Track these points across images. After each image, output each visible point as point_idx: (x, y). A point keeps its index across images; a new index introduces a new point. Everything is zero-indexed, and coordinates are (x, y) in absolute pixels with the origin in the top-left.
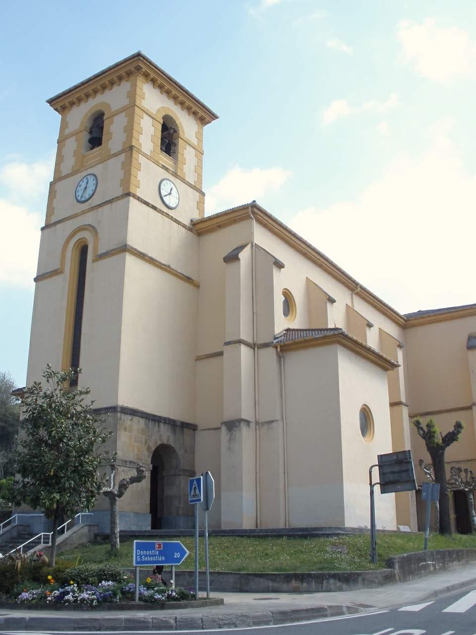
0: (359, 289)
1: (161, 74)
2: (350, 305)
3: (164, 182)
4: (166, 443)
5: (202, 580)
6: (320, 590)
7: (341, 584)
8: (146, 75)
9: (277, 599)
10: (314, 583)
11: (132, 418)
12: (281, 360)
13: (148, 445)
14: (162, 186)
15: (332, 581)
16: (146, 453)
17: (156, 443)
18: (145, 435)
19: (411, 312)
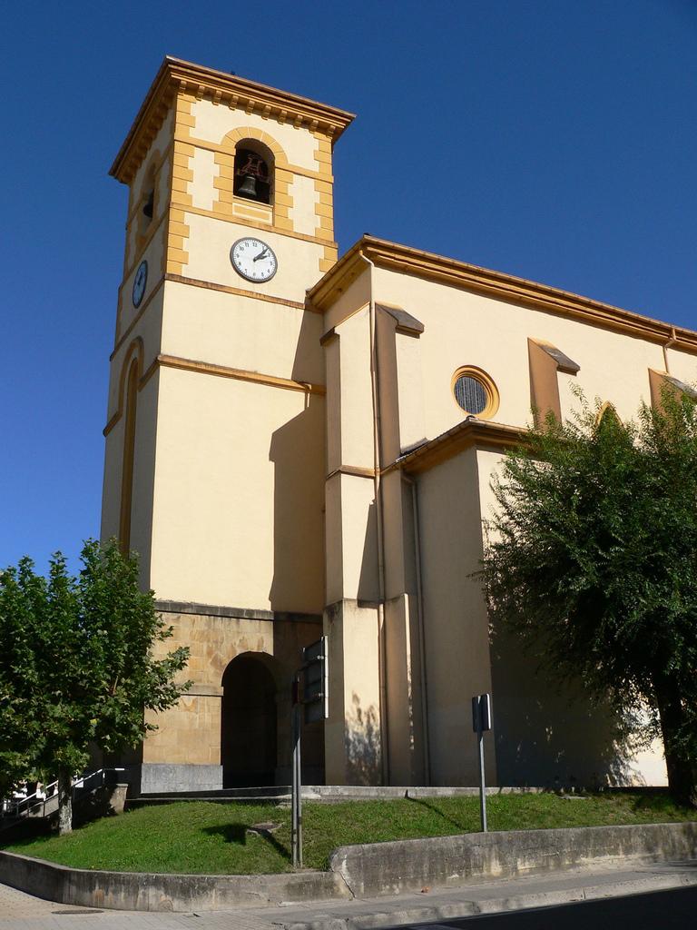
0: (675, 337)
1: (219, 80)
2: (660, 369)
3: (237, 251)
4: (255, 650)
5: (630, 832)
6: (132, 907)
7: (169, 898)
8: (192, 90)
9: (57, 913)
10: (123, 894)
11: (179, 618)
12: (411, 491)
13: (216, 656)
14: (237, 260)
15: (152, 892)
16: (212, 670)
17: (235, 651)
18: (209, 641)
19: (562, 319)
